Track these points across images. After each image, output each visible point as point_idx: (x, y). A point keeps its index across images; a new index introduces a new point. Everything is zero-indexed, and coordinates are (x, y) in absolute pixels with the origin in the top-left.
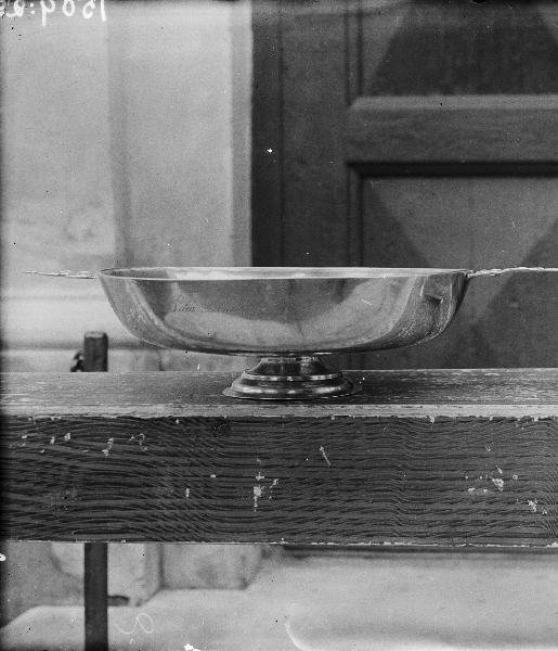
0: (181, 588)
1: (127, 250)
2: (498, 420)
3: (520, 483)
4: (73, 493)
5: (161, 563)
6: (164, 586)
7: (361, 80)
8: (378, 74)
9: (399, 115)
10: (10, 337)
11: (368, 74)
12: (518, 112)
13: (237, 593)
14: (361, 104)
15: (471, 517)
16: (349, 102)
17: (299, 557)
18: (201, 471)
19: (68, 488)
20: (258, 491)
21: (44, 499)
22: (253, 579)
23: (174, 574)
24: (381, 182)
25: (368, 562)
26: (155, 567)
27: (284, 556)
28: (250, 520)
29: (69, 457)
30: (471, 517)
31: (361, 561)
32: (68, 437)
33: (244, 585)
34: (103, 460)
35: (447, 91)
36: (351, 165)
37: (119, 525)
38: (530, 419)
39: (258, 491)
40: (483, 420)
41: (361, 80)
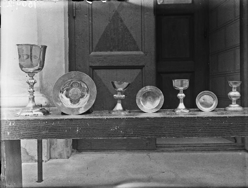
0: (54, 159)
1: (42, 86)
2: (116, 118)
3: (120, 128)
4: (47, 131)
5: (50, 153)
6: (50, 158)
7: (92, 48)
8: (96, 47)
9: (101, 56)
10: (2, 105)
11: (94, 47)
12: (127, 55)
13: (66, 159)
14: (92, 53)
15: (111, 134)
16: (90, 54)
17: (80, 152)
18: (68, 127)
19: (47, 130)
20: (77, 130)
21: (42, 132)
22: (70, 156)
23: (53, 156)
24: (97, 70)
25: (95, 153)
26: (49, 154)
27: (76, 153)
28: (77, 135)
29: (46, 125)
30: (111, 134)
31: (94, 153)
32: (47, 122)
33: (68, 158)
34: (53, 126)
35: (111, 51)
36: (90, 67)
37: (55, 136)
38: (121, 118)
39: (77, 130)
40: (113, 119)
41: (92, 48)
